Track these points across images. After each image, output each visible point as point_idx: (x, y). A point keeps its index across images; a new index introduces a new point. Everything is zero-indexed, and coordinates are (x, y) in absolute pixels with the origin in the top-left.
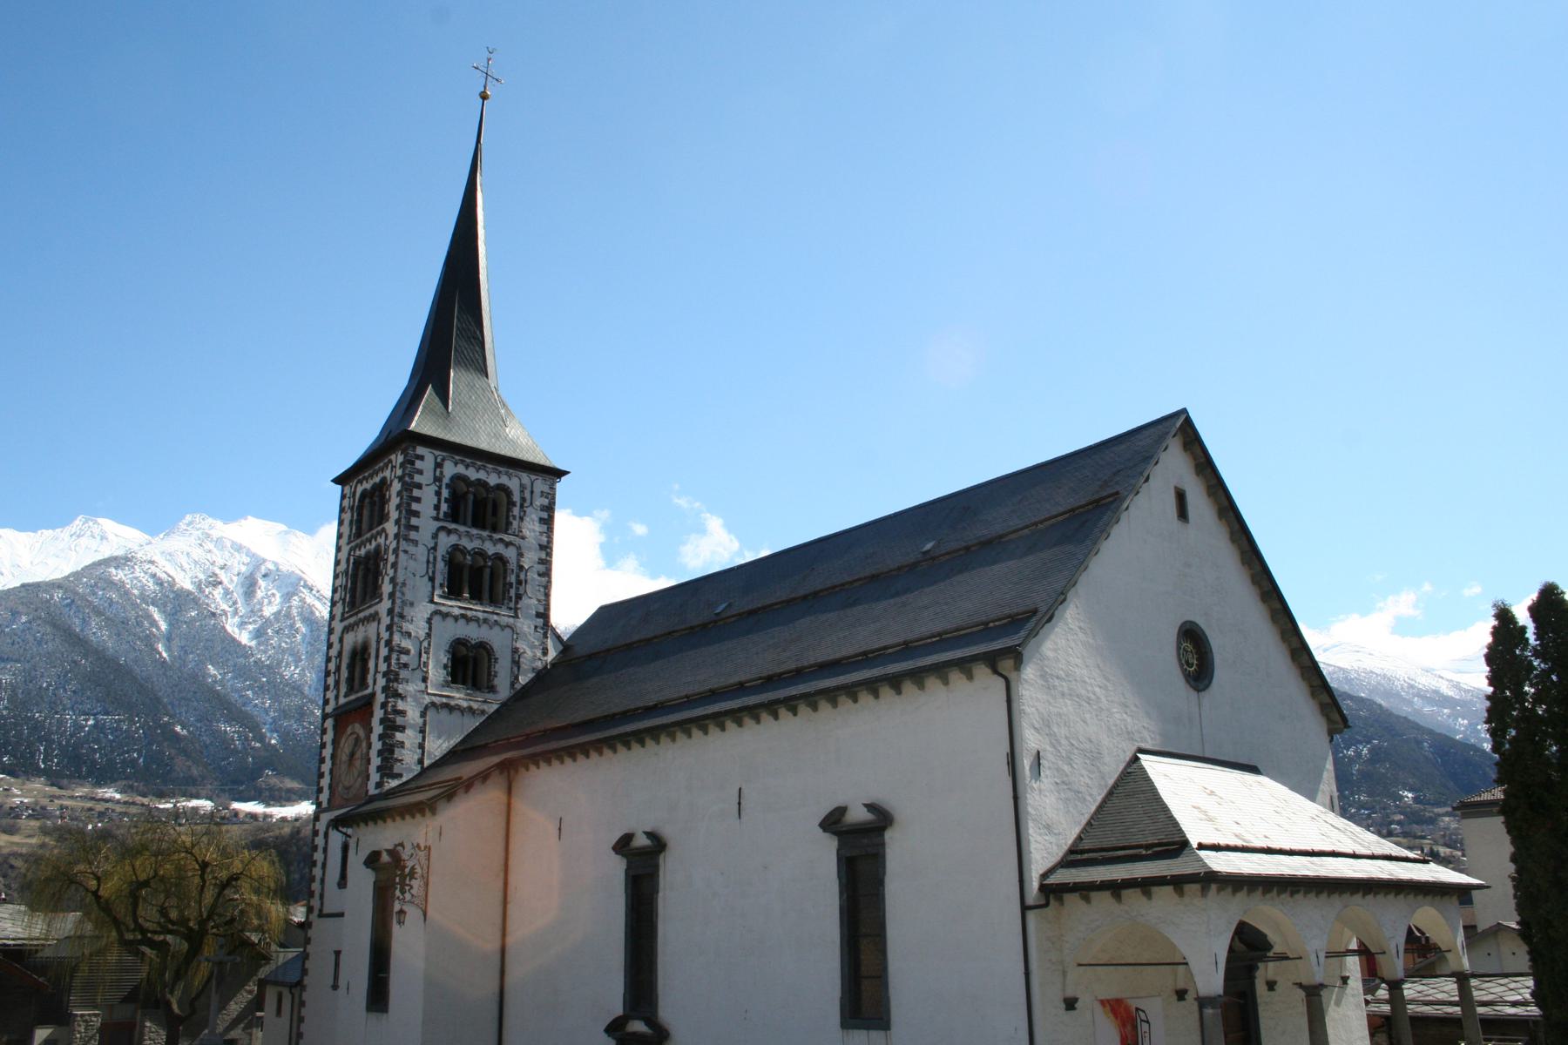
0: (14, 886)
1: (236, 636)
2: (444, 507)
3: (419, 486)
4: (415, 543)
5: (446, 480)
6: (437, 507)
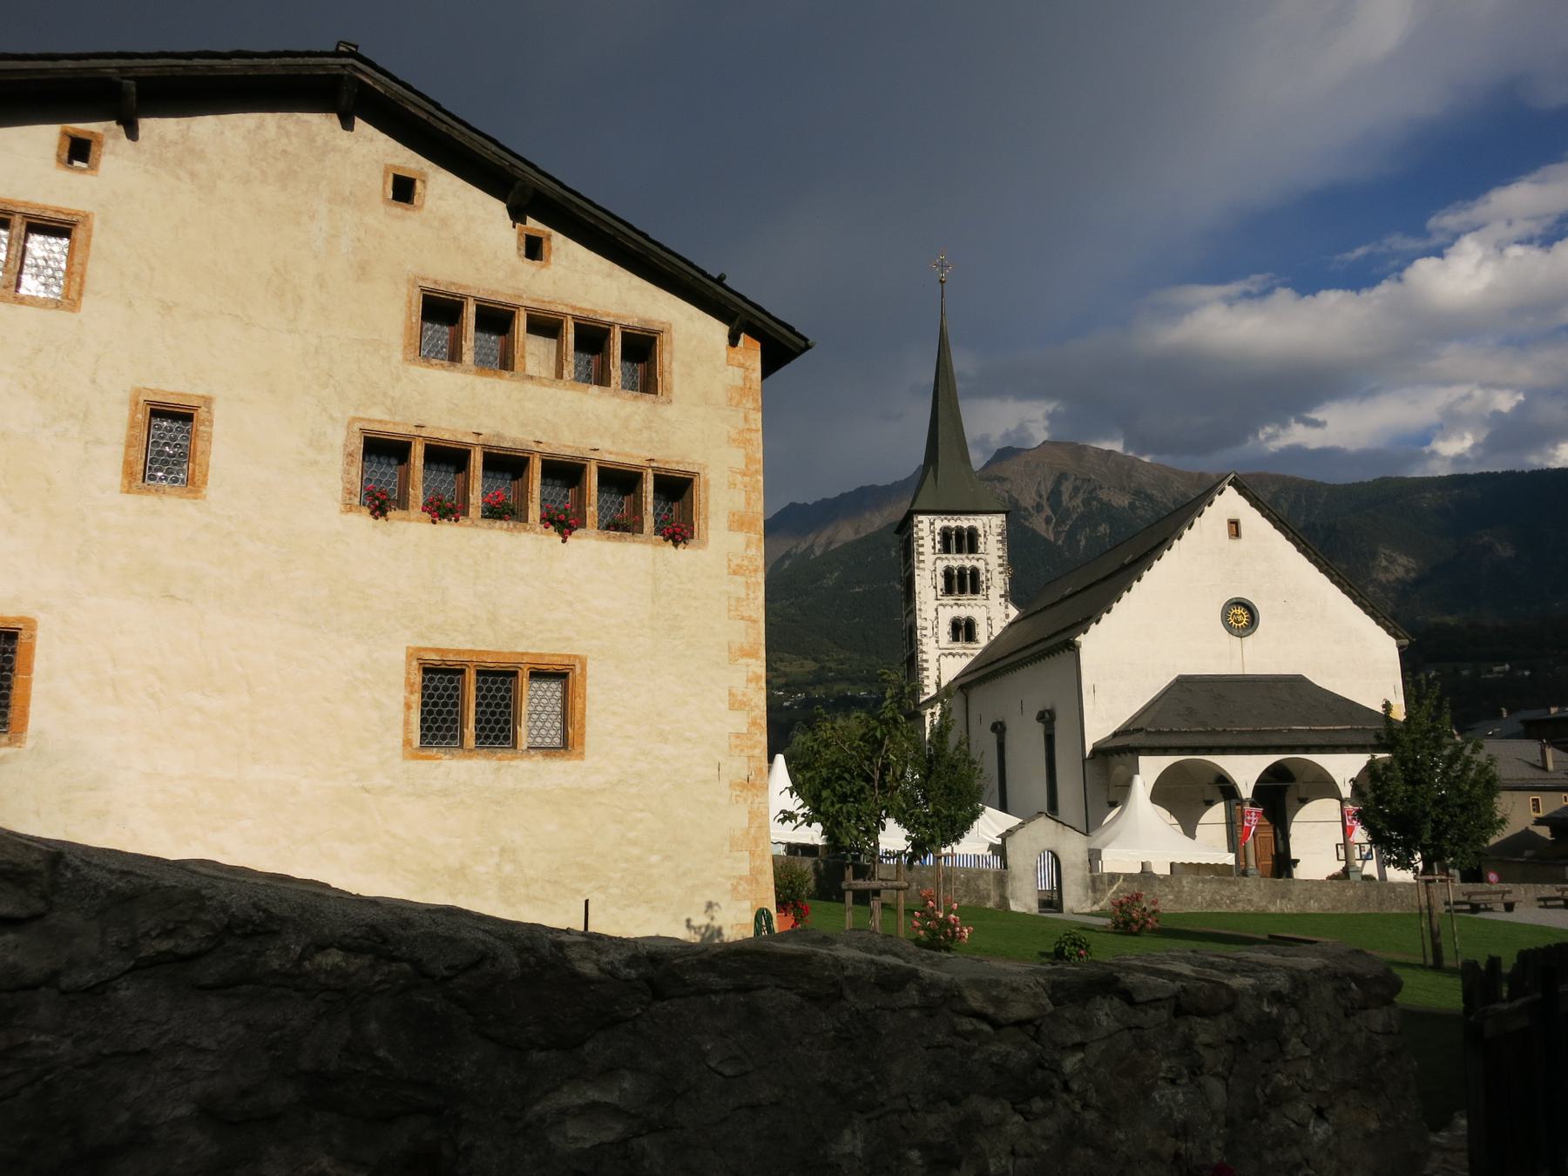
2: (938, 546)
4: (923, 569)
5: (937, 531)
6: (934, 548)
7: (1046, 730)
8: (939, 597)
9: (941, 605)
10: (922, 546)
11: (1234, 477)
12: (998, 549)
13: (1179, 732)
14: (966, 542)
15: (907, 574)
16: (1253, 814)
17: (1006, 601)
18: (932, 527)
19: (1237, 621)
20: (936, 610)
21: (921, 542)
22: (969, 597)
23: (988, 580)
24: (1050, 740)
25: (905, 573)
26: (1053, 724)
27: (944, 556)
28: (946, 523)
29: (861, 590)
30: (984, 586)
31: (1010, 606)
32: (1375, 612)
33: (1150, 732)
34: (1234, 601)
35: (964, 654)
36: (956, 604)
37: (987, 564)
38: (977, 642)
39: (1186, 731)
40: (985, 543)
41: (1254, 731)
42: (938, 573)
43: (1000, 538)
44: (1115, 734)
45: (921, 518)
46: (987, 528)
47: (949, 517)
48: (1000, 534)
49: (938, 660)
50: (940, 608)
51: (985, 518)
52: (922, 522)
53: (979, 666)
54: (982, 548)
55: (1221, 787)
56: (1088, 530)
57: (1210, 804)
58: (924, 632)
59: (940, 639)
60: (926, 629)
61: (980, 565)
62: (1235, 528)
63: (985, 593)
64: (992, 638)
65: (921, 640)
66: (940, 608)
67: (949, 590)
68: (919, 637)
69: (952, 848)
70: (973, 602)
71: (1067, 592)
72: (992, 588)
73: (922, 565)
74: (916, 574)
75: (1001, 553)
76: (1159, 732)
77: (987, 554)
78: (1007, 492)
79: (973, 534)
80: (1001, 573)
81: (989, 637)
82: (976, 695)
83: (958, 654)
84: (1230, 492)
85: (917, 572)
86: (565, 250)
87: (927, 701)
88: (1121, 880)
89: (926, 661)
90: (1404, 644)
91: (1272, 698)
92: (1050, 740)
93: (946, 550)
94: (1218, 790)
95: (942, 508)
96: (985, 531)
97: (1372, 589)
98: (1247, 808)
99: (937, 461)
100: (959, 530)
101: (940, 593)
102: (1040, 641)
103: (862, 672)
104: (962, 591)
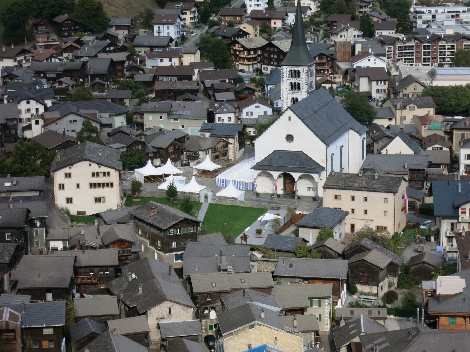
0: (210, 201)
1: (3, 244)
2: (288, 76)
3: (283, 73)
4: (284, 83)
5: (288, 71)
6: (287, 76)
21: (283, 74)
50: (288, 95)
54: (301, 77)
61: (300, 82)
62: (290, 118)
70: (298, 93)
73: (283, 81)
85: (282, 83)
86: (102, 167)
100: (295, 71)
101: (288, 90)
104: (295, 89)
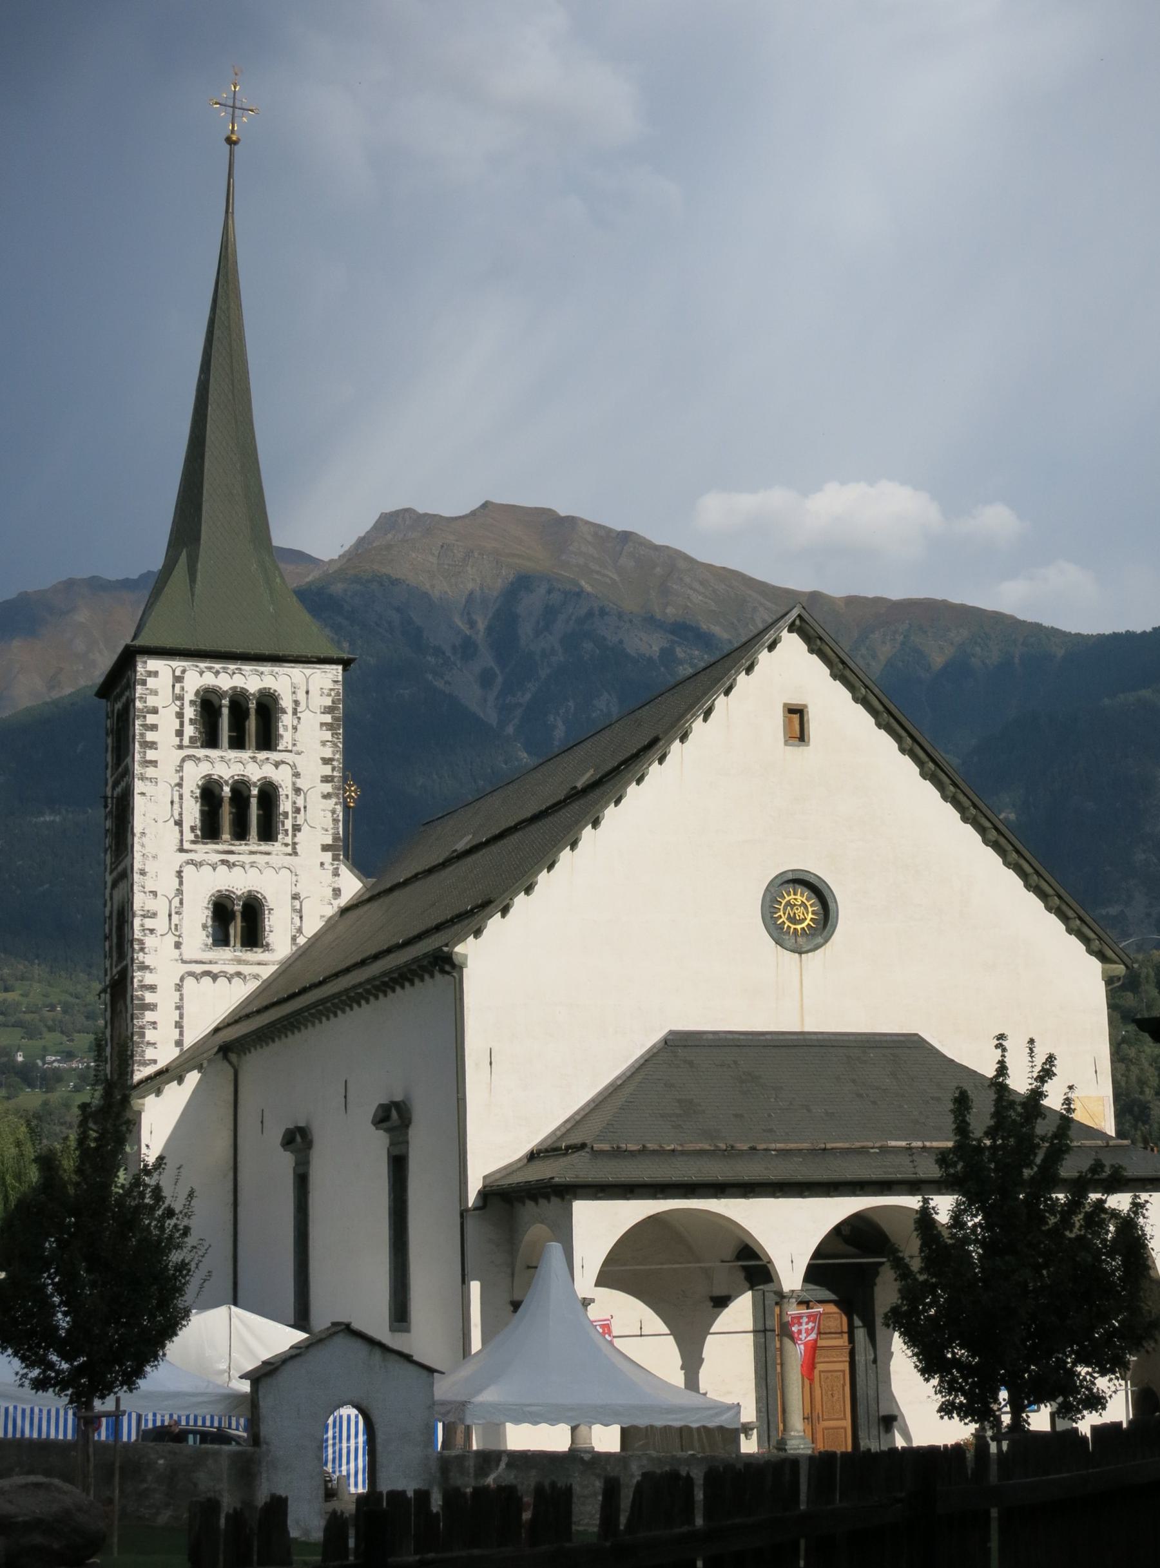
2: (189, 731)
4: (154, 781)
5: (190, 696)
6: (180, 733)
7: (392, 1144)
8: (187, 846)
9: (191, 862)
10: (154, 727)
11: (799, 616)
12: (324, 743)
13: (660, 1153)
14: (252, 724)
15: (119, 790)
16: (805, 1320)
17: (335, 858)
18: (178, 686)
19: (792, 919)
20: (179, 874)
21: (151, 719)
22: (255, 848)
23: (297, 811)
24: (398, 1166)
25: (114, 788)
26: (407, 1134)
27: (201, 753)
28: (209, 680)
29: (58, 819)
30: (288, 824)
31: (344, 870)
32: (1064, 907)
33: (602, 1152)
34: (790, 876)
35: (238, 974)
36: (223, 862)
37: (297, 775)
38: (267, 947)
39: (673, 1151)
40: (295, 728)
41: (812, 1151)
42: (186, 792)
43: (328, 718)
44: (533, 1156)
45: (153, 664)
46: (301, 696)
47: (217, 666)
48: (329, 710)
49: (179, 987)
50: (189, 871)
51: (297, 673)
52: (155, 674)
53: (265, 1003)
54: (286, 738)
55: (744, 1268)
56: (571, 704)
57: (721, 1302)
58: (149, 924)
59: (185, 941)
60: (154, 915)
61: (282, 777)
63: (289, 840)
64: (301, 941)
65: (141, 942)
66: (189, 871)
67: (210, 830)
68: (137, 934)
69: (118, 1400)
71: (461, 845)
72: (305, 828)
73: (150, 772)
74: (136, 791)
75: (328, 752)
76: (617, 1153)
77: (299, 753)
78: (398, 610)
79: (268, 706)
80: (327, 796)
81: (294, 938)
82: (254, 1063)
83: (224, 974)
84: (792, 644)
87: (149, 1079)
88: (503, 1465)
89: (152, 988)
90: (1117, 973)
91: (854, 1081)
92: (398, 1166)
93: (211, 741)
94: (741, 1275)
95: (203, 646)
96: (296, 703)
97: (1143, 857)
98: (793, 1310)
99: (197, 539)
100: (238, 700)
101: (189, 836)
102: (389, 951)
103: (52, 1008)
104: (241, 834)
